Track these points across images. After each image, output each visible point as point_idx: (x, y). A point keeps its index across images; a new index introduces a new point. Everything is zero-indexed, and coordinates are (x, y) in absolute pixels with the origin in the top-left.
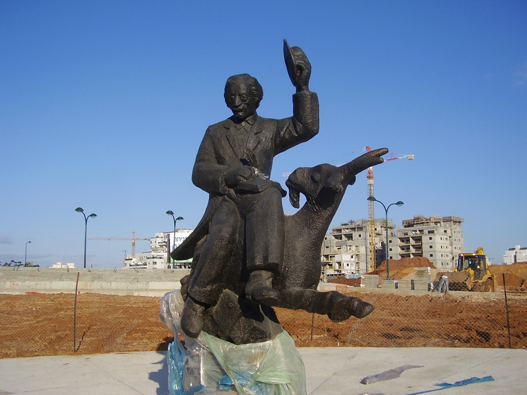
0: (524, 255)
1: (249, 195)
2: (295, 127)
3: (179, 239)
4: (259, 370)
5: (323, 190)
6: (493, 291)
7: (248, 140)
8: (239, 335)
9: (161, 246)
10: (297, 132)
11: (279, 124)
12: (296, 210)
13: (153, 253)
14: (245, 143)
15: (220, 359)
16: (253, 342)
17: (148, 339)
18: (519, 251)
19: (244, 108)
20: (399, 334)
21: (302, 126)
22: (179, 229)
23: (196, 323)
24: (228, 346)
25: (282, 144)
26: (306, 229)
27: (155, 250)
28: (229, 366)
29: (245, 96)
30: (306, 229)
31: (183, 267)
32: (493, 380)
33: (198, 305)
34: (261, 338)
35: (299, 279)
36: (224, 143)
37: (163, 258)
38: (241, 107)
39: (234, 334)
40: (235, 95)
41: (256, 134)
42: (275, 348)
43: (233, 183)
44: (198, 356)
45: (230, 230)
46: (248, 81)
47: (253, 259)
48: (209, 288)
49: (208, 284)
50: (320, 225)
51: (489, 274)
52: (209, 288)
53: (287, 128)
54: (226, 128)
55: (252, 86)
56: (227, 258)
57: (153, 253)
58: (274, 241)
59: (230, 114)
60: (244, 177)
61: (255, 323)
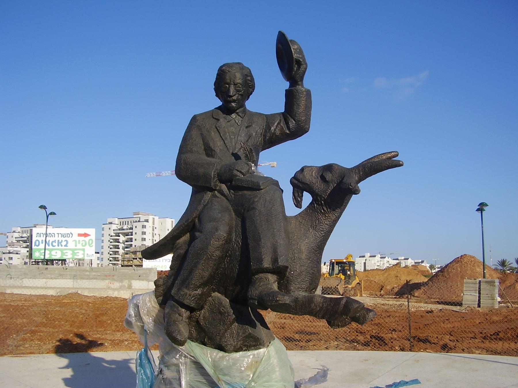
0: (373, 262)
1: (246, 192)
2: (287, 123)
3: (42, 235)
4: (253, 380)
5: (331, 192)
6: (361, 295)
7: (234, 133)
8: (232, 342)
9: (18, 241)
10: (288, 128)
11: (269, 119)
12: (298, 211)
13: (9, 248)
14: (236, 137)
15: (209, 370)
16: (245, 350)
17: (39, 340)
18: (368, 259)
19: (237, 99)
20: (297, 337)
21: (292, 122)
22: (38, 225)
23: (183, 329)
24: (218, 354)
25: (271, 141)
26: (311, 230)
27: (12, 245)
28: (220, 376)
29: (240, 86)
30: (311, 230)
31: (40, 263)
32: (420, 383)
33: (183, 310)
34: (254, 346)
35: (304, 283)
36: (213, 134)
37: (20, 254)
38: (235, 98)
39: (225, 342)
40: (229, 84)
41: (247, 127)
42: (269, 358)
43: (227, 178)
44: (177, 365)
45: (227, 228)
46: (244, 71)
47: (260, 260)
48: (199, 291)
49: (199, 287)
50: (326, 227)
51: (357, 280)
52: (199, 291)
53: (278, 124)
54: (215, 119)
55: (248, 76)
56: (222, 259)
57: (9, 248)
58: (282, 242)
59: (219, 103)
60: (241, 172)
61: (250, 330)
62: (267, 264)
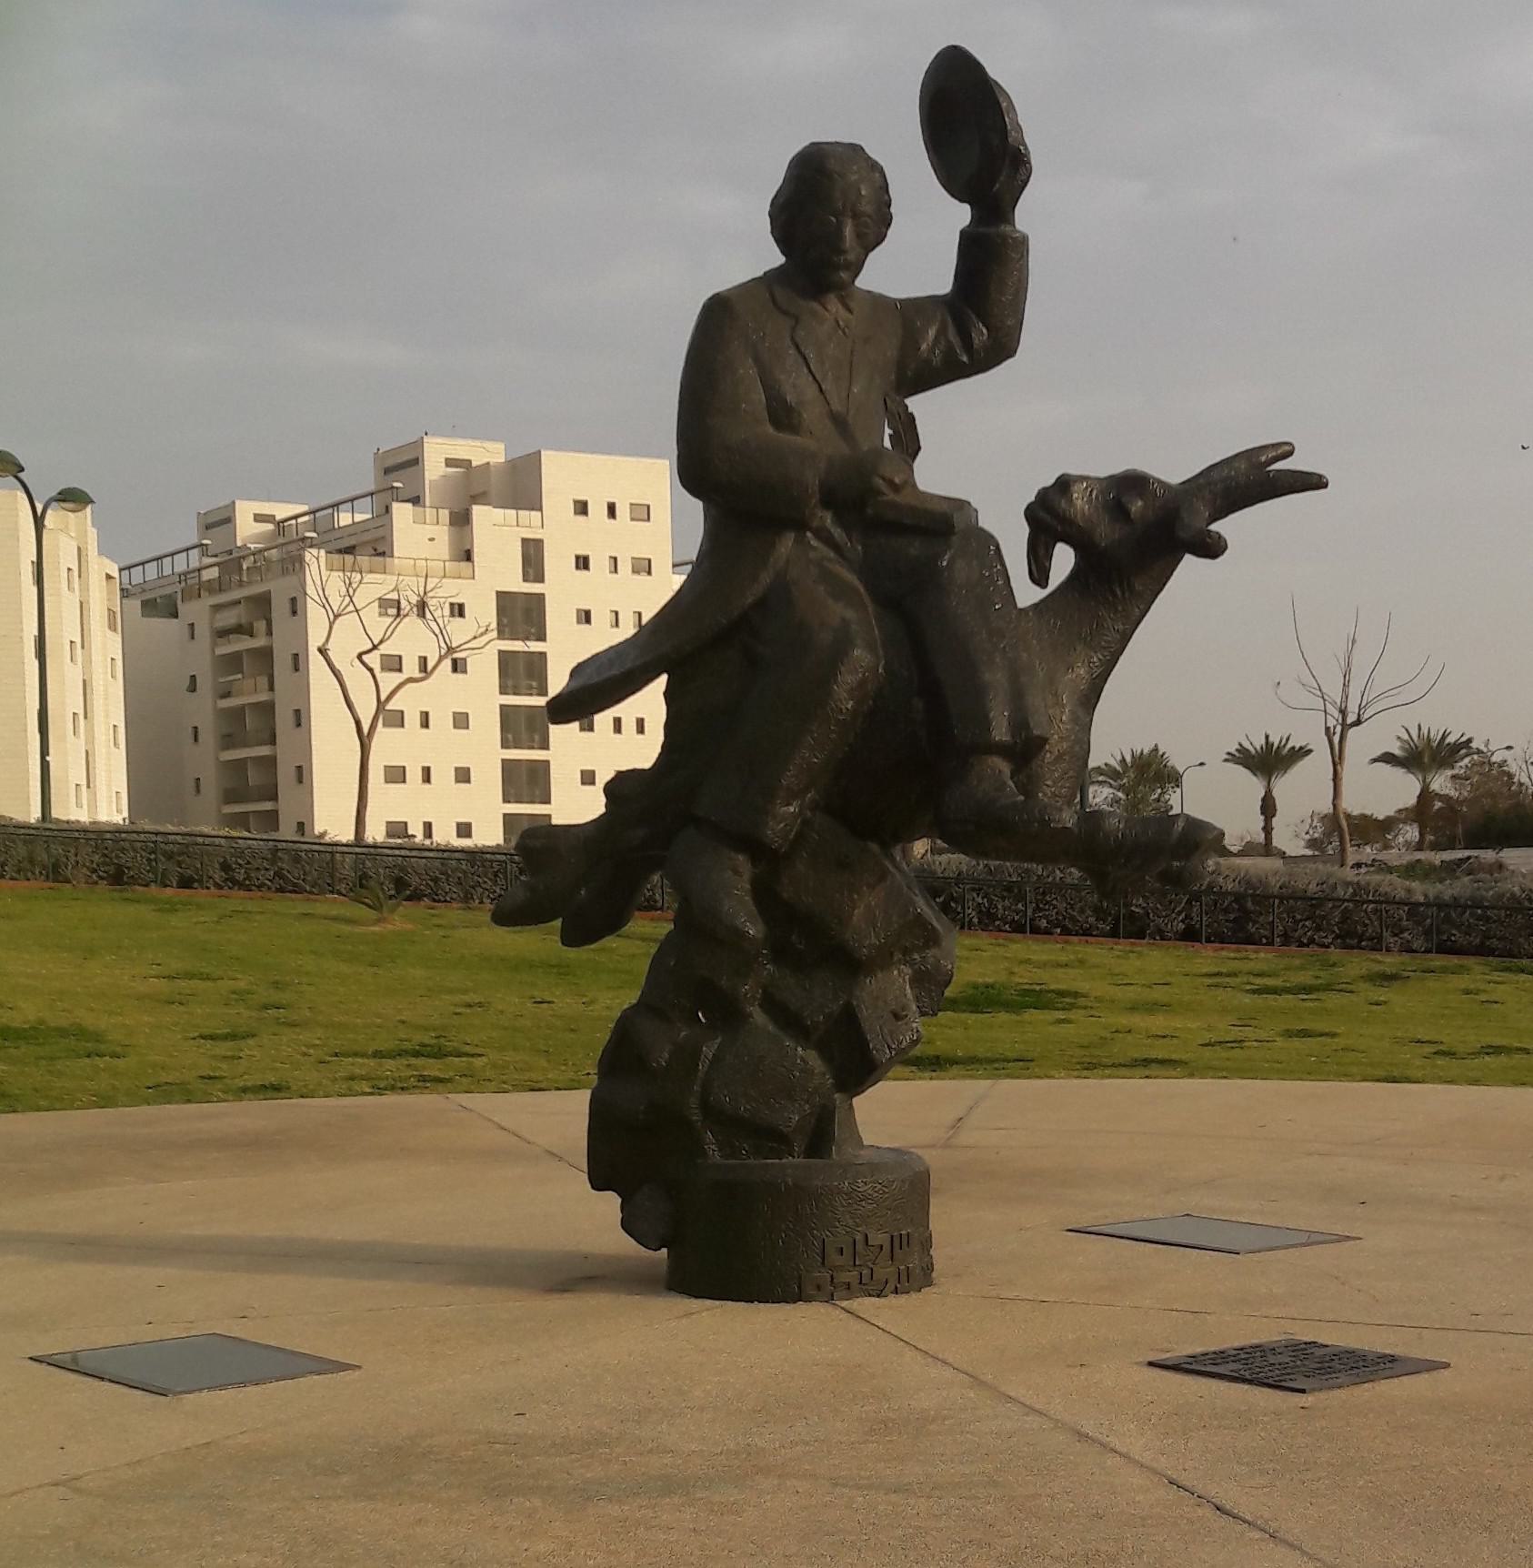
11: (912, 311)
47: (985, 724)
62: (1000, 732)
